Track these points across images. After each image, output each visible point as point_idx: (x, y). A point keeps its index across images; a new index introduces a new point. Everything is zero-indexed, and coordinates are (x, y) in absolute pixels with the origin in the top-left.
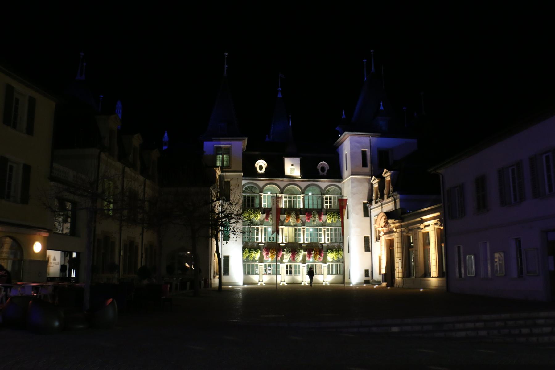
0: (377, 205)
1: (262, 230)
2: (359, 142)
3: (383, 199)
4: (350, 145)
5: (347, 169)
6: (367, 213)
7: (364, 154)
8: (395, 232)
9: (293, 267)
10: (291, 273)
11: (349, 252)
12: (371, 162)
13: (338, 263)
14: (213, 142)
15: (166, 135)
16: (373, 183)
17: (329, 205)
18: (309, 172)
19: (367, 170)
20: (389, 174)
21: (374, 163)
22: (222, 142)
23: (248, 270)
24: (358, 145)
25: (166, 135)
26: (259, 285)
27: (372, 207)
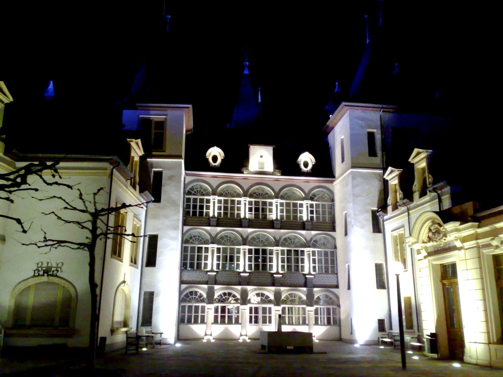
0: (396, 212)
1: (213, 251)
2: (363, 119)
3: (411, 199)
4: (346, 127)
5: (343, 160)
6: (377, 227)
7: (371, 136)
8: (460, 249)
9: (260, 311)
10: (256, 322)
11: (349, 288)
12: (383, 149)
13: (331, 307)
14: (138, 111)
15: (51, 86)
16: (388, 178)
17: (315, 215)
18: (286, 164)
19: (378, 160)
20: (423, 155)
21: (390, 149)
22: (152, 112)
23: (187, 316)
24: (361, 122)
25: (51, 86)
26: (205, 341)
27: (386, 217)
